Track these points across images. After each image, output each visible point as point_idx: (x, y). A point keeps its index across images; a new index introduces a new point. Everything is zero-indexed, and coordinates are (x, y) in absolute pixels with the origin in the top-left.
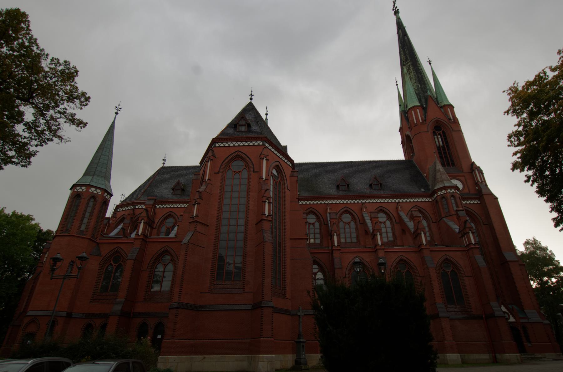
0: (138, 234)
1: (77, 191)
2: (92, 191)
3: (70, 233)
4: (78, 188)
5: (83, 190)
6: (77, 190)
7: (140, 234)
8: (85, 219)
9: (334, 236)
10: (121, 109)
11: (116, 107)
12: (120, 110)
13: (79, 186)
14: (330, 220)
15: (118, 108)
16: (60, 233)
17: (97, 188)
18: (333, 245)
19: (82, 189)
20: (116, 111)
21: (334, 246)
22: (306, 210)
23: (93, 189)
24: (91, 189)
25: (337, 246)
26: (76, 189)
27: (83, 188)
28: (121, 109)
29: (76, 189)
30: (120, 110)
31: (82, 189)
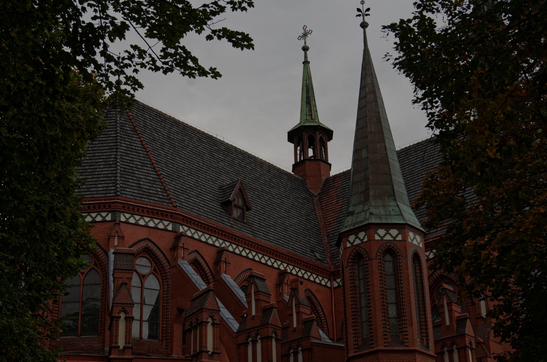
0: (482, 318)
1: (352, 245)
2: (382, 238)
3: (372, 346)
4: (352, 238)
5: (362, 240)
6: (352, 244)
7: (485, 317)
8: (108, 351)
9: (117, 321)
10: (368, 10)
11: (359, 10)
12: (367, 13)
13: (361, 231)
14: (113, 275)
15: (362, 9)
16: (355, 350)
17: (388, 226)
18: (113, 345)
19: (359, 239)
20: (360, 19)
21: (115, 347)
22: (131, 247)
23: (382, 232)
24: (378, 234)
25: (124, 348)
26: (350, 242)
27: (362, 235)
28: (368, 10)
29: (350, 242)
30: (367, 13)
31: (359, 239)
